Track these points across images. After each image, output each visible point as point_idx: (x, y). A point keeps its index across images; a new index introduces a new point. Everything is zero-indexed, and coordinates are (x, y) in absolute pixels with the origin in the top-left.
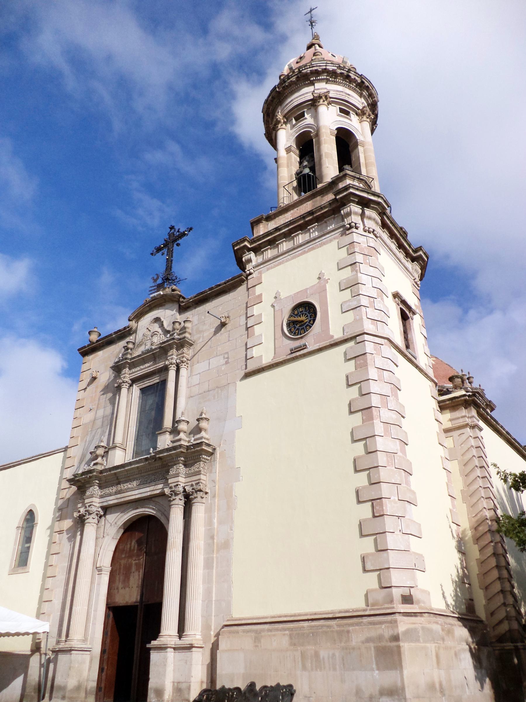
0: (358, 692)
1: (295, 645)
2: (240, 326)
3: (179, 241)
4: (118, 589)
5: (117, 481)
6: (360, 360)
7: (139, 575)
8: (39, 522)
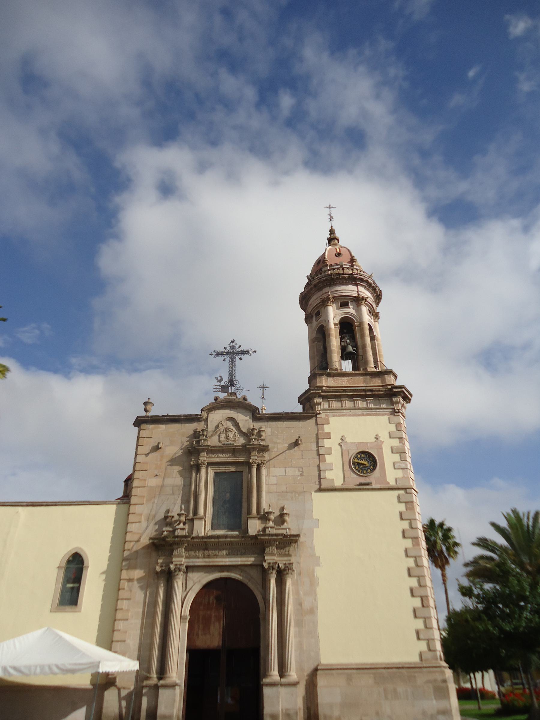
0: (424, 713)
2: (311, 450)
3: (242, 356)
4: (197, 635)
8: (90, 565)
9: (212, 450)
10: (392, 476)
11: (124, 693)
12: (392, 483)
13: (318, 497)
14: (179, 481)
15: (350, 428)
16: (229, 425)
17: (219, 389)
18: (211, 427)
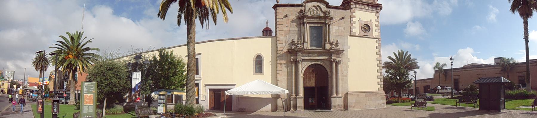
9: (308, 17)
10: (375, 34)
11: (283, 100)
12: (375, 36)
13: (349, 38)
14: (296, 29)
15: (362, 15)
16: (314, 8)
18: (307, 9)
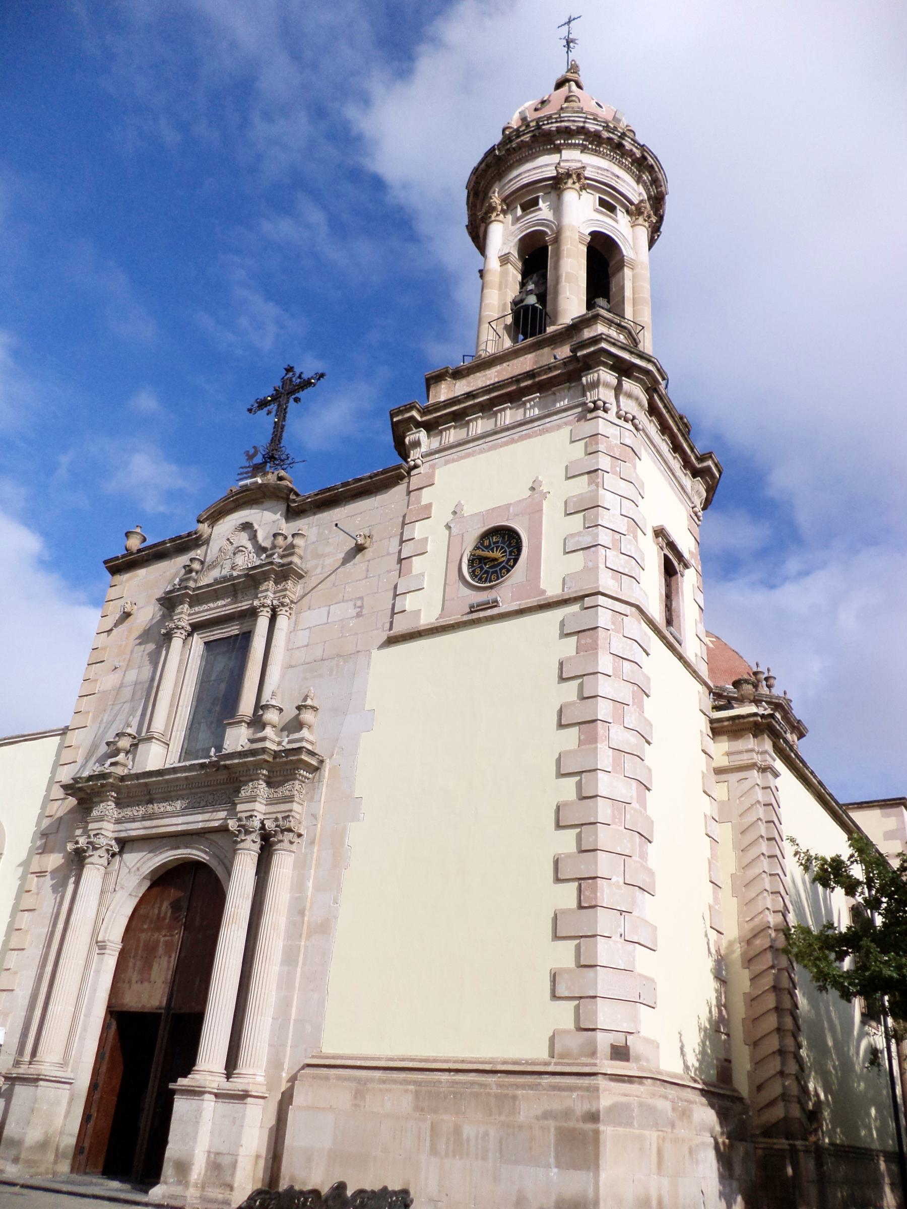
0: (520, 1203)
1: (422, 1110)
2: (389, 554)
4: (130, 982)
5: (148, 797)
6: (586, 639)
7: (169, 962)
17: (246, 473)
